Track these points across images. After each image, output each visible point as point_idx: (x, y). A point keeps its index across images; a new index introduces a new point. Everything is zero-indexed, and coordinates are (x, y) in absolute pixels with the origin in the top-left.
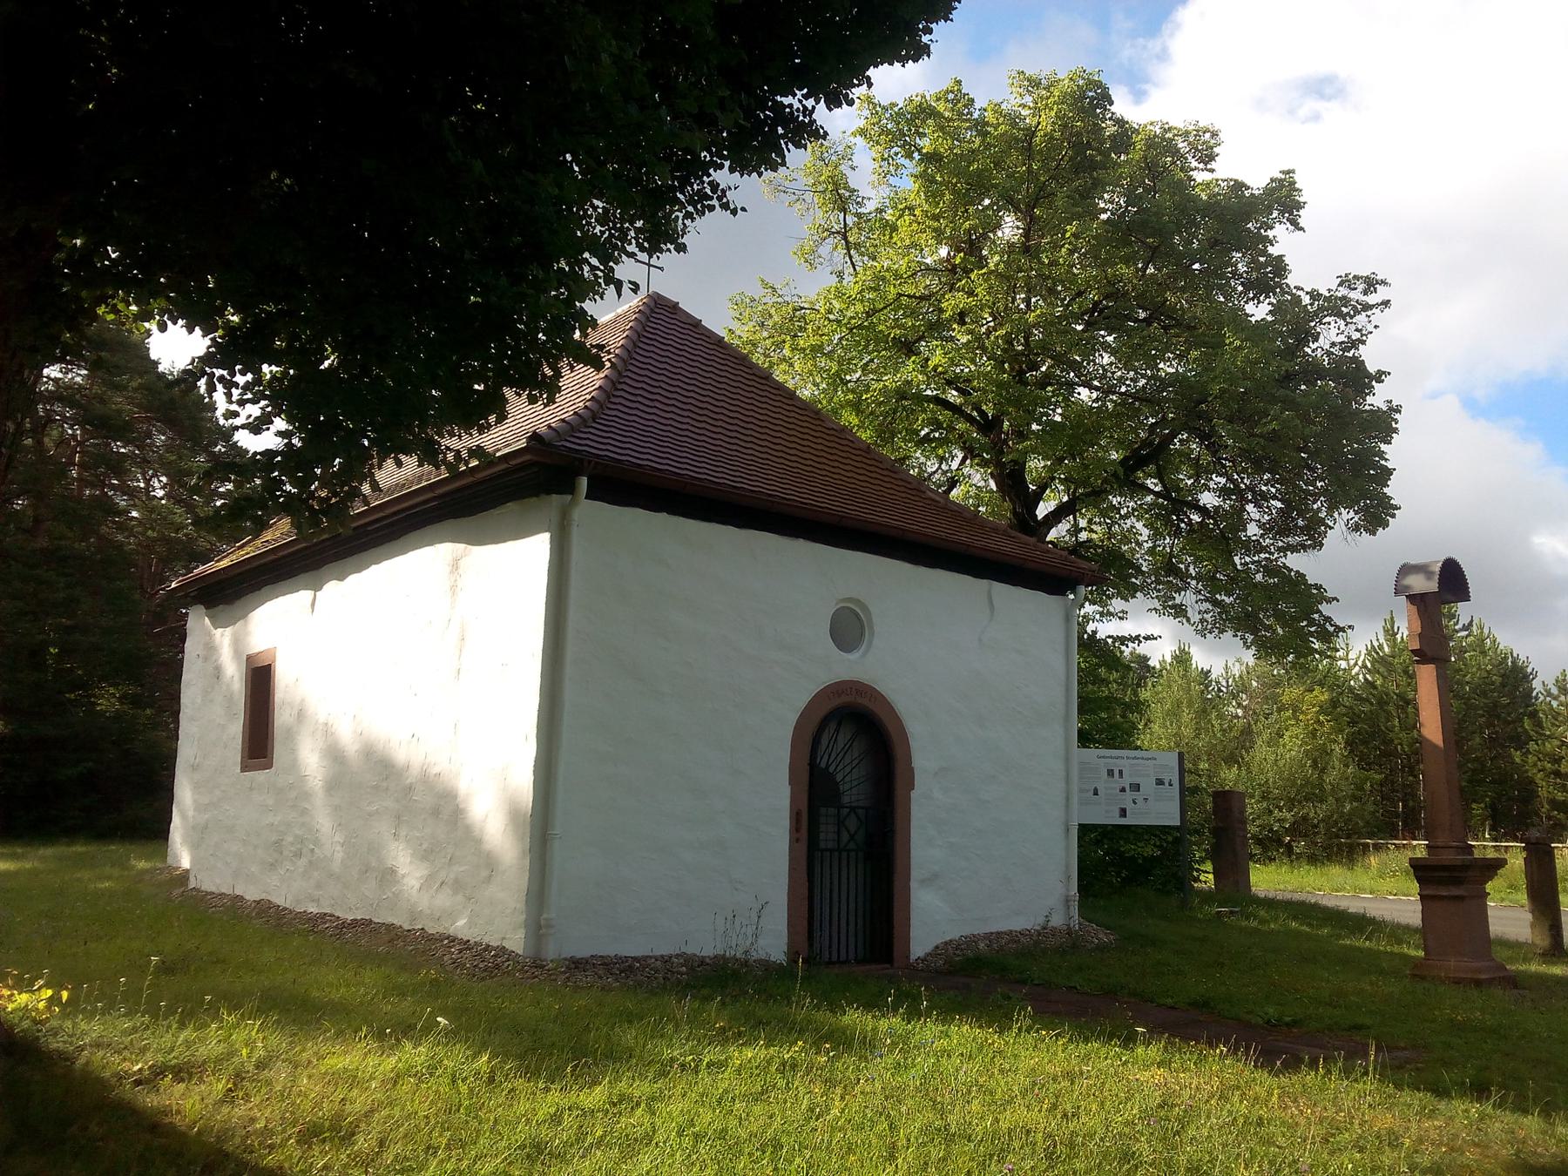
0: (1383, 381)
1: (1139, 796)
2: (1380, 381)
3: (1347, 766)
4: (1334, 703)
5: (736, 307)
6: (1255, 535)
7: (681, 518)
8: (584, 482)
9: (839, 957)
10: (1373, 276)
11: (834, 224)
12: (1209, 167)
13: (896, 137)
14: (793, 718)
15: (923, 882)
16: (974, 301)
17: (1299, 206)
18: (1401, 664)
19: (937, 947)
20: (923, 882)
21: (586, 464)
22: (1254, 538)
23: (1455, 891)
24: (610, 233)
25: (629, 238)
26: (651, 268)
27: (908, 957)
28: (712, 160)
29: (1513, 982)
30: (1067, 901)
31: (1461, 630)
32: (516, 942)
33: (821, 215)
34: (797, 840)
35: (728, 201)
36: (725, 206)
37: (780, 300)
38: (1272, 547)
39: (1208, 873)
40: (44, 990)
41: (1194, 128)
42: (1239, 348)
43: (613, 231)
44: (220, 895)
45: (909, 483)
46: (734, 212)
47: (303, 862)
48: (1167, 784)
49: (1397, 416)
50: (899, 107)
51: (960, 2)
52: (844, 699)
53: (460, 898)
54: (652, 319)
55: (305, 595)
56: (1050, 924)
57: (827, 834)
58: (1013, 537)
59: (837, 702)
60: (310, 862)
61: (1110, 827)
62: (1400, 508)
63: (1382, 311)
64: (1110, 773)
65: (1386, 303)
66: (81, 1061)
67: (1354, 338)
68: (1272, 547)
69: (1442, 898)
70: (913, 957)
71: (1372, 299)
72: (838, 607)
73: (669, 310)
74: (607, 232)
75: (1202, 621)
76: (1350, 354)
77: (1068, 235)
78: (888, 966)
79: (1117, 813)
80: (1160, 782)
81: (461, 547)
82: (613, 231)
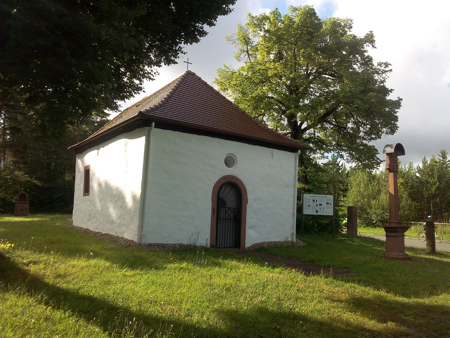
0: (392, 92)
1: (322, 207)
2: (391, 92)
3: (408, 201)
4: (407, 183)
5: (218, 72)
6: (362, 135)
7: (182, 133)
8: (154, 124)
9: (229, 246)
10: (387, 63)
11: (245, 49)
12: (350, 30)
13: (256, 26)
14: (213, 185)
15: (249, 228)
16: (276, 71)
17: (374, 41)
18: (427, 171)
19: (253, 245)
20: (249, 228)
21: (154, 119)
22: (362, 136)
23: (394, 234)
24: (157, 60)
25: (162, 61)
26: (188, 64)
27: (245, 247)
28: (179, 41)
29: (409, 258)
30: (293, 234)
31: (448, 162)
32: (136, 239)
33: (241, 46)
34: (213, 216)
35: (182, 51)
36: (182, 52)
37: (229, 70)
38: (367, 139)
39: (346, 229)
40: (8, 244)
41: (346, 19)
42: (348, 84)
43: (157, 59)
44: (79, 227)
45: (255, 122)
46: (184, 54)
47: (95, 219)
48: (330, 204)
49: (401, 101)
50: (258, 17)
51: (237, 1)
52: (228, 180)
53: (126, 228)
54: (186, 78)
55: (96, 151)
56: (288, 240)
57: (222, 215)
58: (282, 137)
59: (225, 181)
60: (97, 219)
61: (316, 216)
62: (399, 127)
63: (390, 72)
64: (314, 201)
65: (391, 70)
66: (12, 259)
67: (382, 80)
68: (367, 139)
69: (391, 236)
70: (246, 247)
71: (387, 69)
72: (227, 156)
73: (192, 75)
74: (156, 60)
75: (347, 159)
76: (382, 85)
77: (301, 53)
78: (239, 249)
79: (315, 211)
80: (328, 203)
81: (127, 140)
82: (157, 59)
